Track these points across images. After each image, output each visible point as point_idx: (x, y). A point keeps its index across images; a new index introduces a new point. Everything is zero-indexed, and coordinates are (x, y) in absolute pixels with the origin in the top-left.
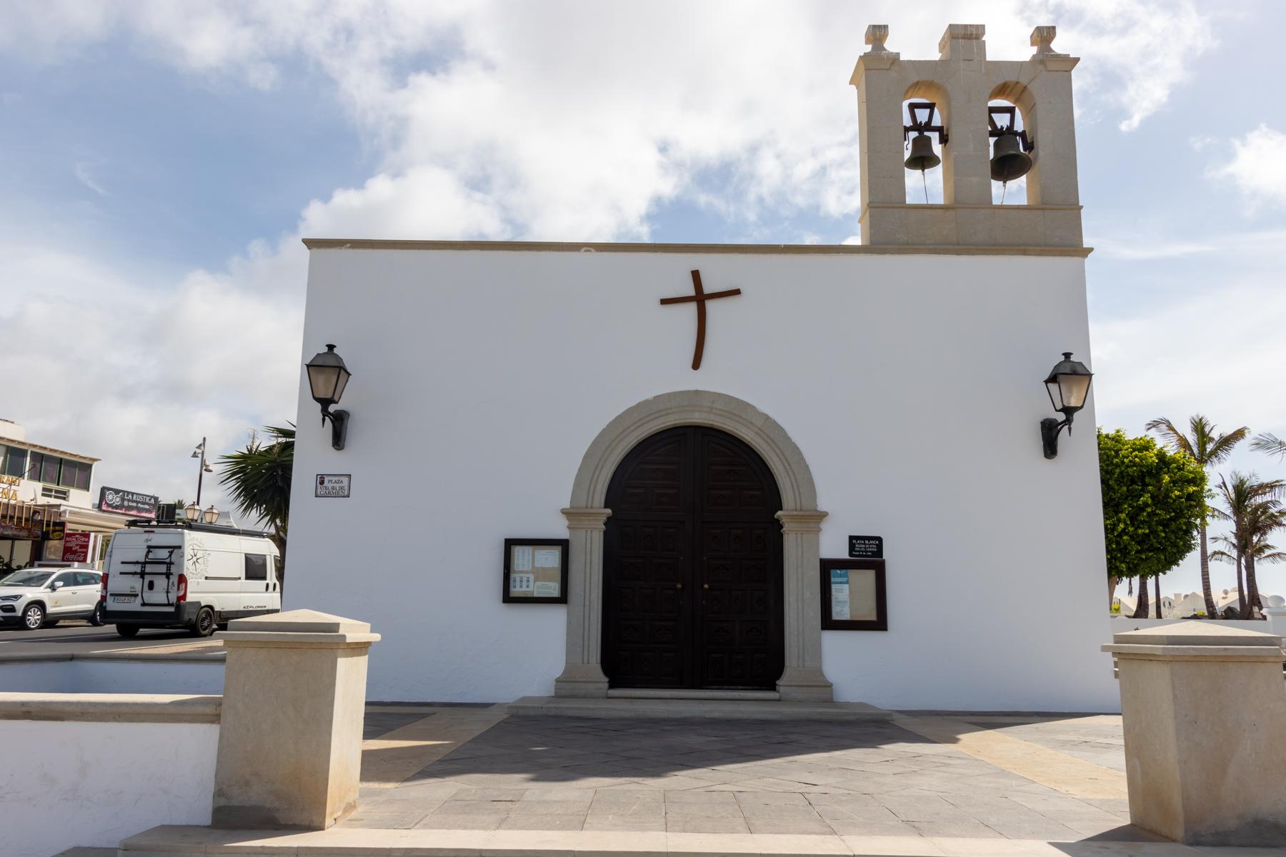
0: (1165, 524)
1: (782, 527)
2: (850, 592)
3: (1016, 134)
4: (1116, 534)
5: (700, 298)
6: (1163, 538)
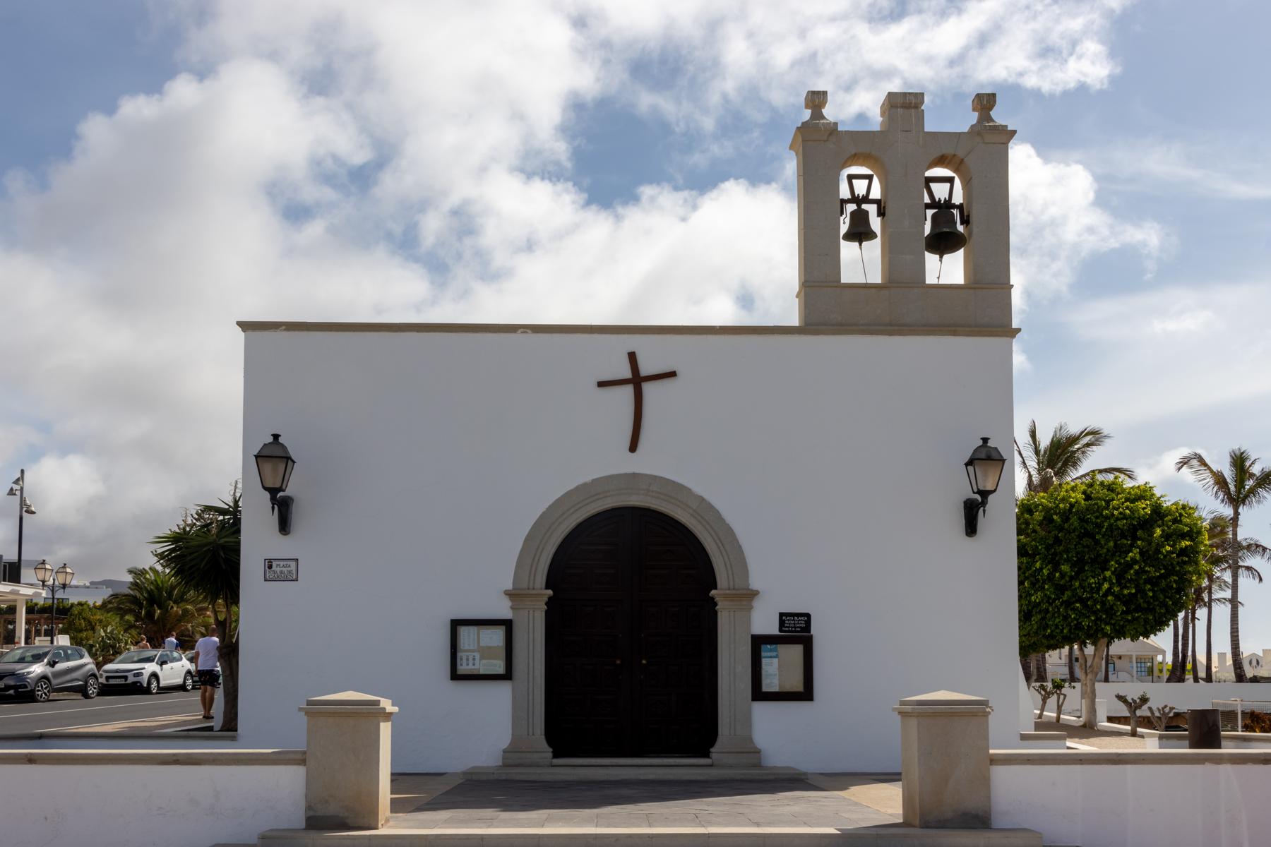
0: (1154, 582)
1: (716, 604)
2: (780, 666)
3: (954, 206)
4: (1101, 593)
5: (637, 380)
6: (1151, 597)
